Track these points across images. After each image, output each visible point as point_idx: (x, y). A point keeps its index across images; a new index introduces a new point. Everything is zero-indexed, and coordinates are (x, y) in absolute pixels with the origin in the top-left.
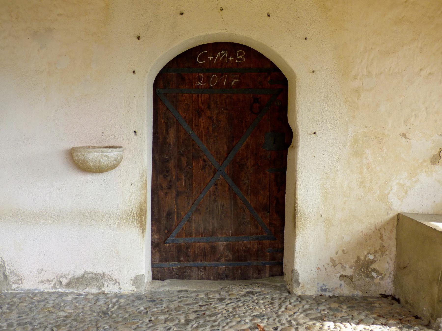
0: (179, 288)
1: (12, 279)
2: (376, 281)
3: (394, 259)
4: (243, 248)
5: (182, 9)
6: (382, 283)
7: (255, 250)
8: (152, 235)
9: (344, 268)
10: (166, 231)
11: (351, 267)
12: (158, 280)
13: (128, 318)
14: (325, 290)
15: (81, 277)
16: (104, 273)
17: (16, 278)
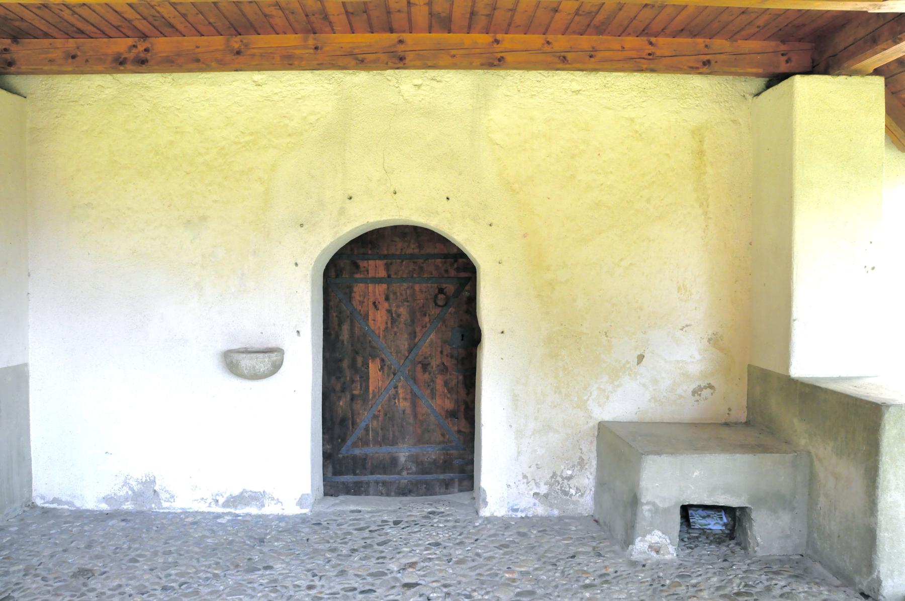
0: (351, 507)
1: (163, 496)
2: (574, 498)
3: (594, 473)
4: (427, 459)
5: (350, 193)
6: (581, 500)
7: (441, 461)
8: (323, 445)
9: (537, 484)
10: (340, 440)
11: (545, 484)
12: (332, 496)
13: (222, 577)
14: (516, 510)
15: (240, 495)
16: (264, 492)
17: (168, 496)
